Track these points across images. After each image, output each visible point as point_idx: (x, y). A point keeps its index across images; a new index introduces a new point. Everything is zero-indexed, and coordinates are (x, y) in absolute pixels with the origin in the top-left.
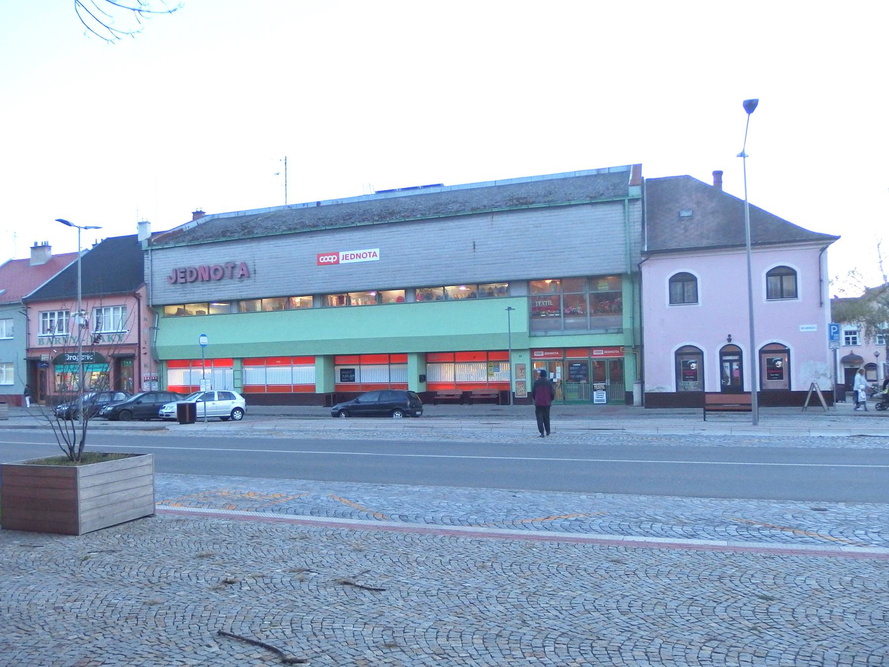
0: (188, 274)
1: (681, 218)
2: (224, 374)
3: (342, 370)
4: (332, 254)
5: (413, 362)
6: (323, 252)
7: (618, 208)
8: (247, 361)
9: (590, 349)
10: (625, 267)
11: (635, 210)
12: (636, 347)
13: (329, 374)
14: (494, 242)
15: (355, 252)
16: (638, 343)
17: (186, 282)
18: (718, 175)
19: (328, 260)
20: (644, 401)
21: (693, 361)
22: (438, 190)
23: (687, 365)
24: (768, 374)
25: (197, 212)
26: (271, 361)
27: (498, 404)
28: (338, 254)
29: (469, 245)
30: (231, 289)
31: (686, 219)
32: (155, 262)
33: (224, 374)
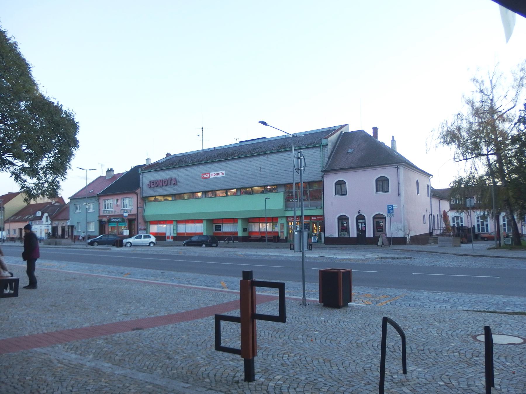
0: (155, 183)
2: (170, 227)
3: (216, 226)
4: (207, 174)
5: (240, 222)
6: (204, 173)
7: (319, 149)
8: (178, 222)
11: (325, 150)
13: (208, 228)
15: (215, 173)
17: (154, 187)
18: (375, 130)
19: (206, 176)
22: (265, 140)
23: (378, 223)
25: (168, 154)
28: (209, 174)
30: (170, 190)
31: (350, 153)
32: (144, 178)
33: (170, 227)
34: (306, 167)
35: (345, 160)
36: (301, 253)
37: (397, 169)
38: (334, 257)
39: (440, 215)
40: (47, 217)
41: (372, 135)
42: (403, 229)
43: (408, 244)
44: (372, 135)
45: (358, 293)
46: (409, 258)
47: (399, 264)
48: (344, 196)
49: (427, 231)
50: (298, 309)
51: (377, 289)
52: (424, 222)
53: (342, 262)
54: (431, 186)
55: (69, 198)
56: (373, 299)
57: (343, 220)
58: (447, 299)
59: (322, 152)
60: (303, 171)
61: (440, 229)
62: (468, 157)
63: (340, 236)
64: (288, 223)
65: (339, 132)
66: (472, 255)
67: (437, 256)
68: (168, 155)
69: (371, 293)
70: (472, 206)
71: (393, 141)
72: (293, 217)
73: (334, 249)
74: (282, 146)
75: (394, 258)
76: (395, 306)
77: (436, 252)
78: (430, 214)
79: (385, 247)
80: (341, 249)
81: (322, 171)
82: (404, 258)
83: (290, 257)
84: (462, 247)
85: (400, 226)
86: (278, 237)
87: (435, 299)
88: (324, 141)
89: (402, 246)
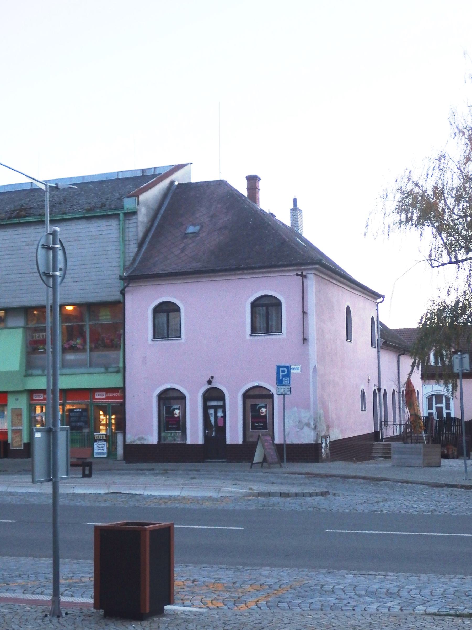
1: (186, 235)
7: (114, 223)
11: (131, 225)
21: (176, 407)
23: (256, 409)
24: (253, 423)
31: (191, 235)
34: (67, 272)
35: (179, 251)
36: (51, 483)
37: (300, 278)
38: (147, 493)
39: (399, 392)
41: (245, 193)
42: (312, 423)
43: (323, 461)
44: (245, 193)
45: (194, 581)
46: (322, 494)
47: (298, 508)
48: (174, 342)
49: (370, 429)
50: (40, 625)
51: (239, 569)
52: (363, 408)
53: (163, 506)
54: (380, 319)
56: (227, 595)
57: (172, 401)
58: (396, 590)
59: (124, 229)
60: (59, 279)
61: (398, 423)
62: (460, 258)
63: (162, 442)
64: (32, 409)
65: (165, 183)
66: (462, 487)
67: (387, 490)
69: (224, 581)
70: (465, 371)
71: (295, 209)
72: (43, 391)
73: (147, 472)
74: (21, 210)
75: (287, 495)
76: (277, 610)
77: (385, 480)
78: (376, 388)
79: (269, 468)
80: (165, 472)
81: (121, 278)
82: (311, 495)
83: (35, 495)
84: (445, 466)
85: (305, 416)
86: (6, 444)
87: (369, 590)
88: (129, 204)
89: (310, 465)
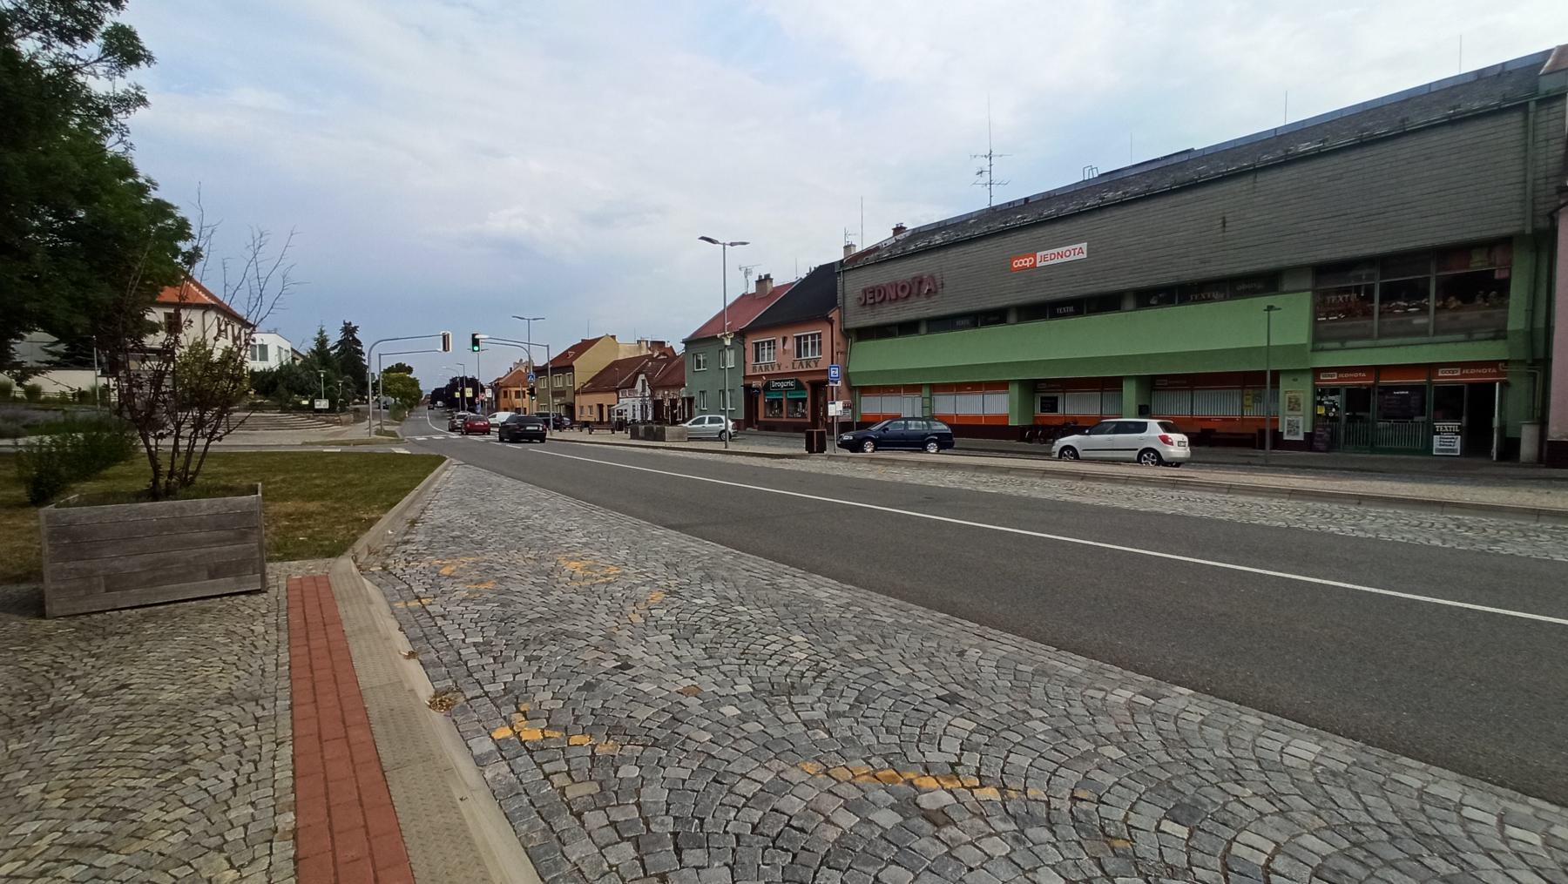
8: (935, 388)
9: (1432, 368)
10: (1520, 222)
12: (1535, 362)
14: (1257, 214)
16: (1540, 355)
20: (1545, 454)
26: (960, 388)
27: (1254, 448)
29: (1216, 222)
32: (847, 284)
40: (643, 381)
55: (685, 342)
68: (898, 230)
